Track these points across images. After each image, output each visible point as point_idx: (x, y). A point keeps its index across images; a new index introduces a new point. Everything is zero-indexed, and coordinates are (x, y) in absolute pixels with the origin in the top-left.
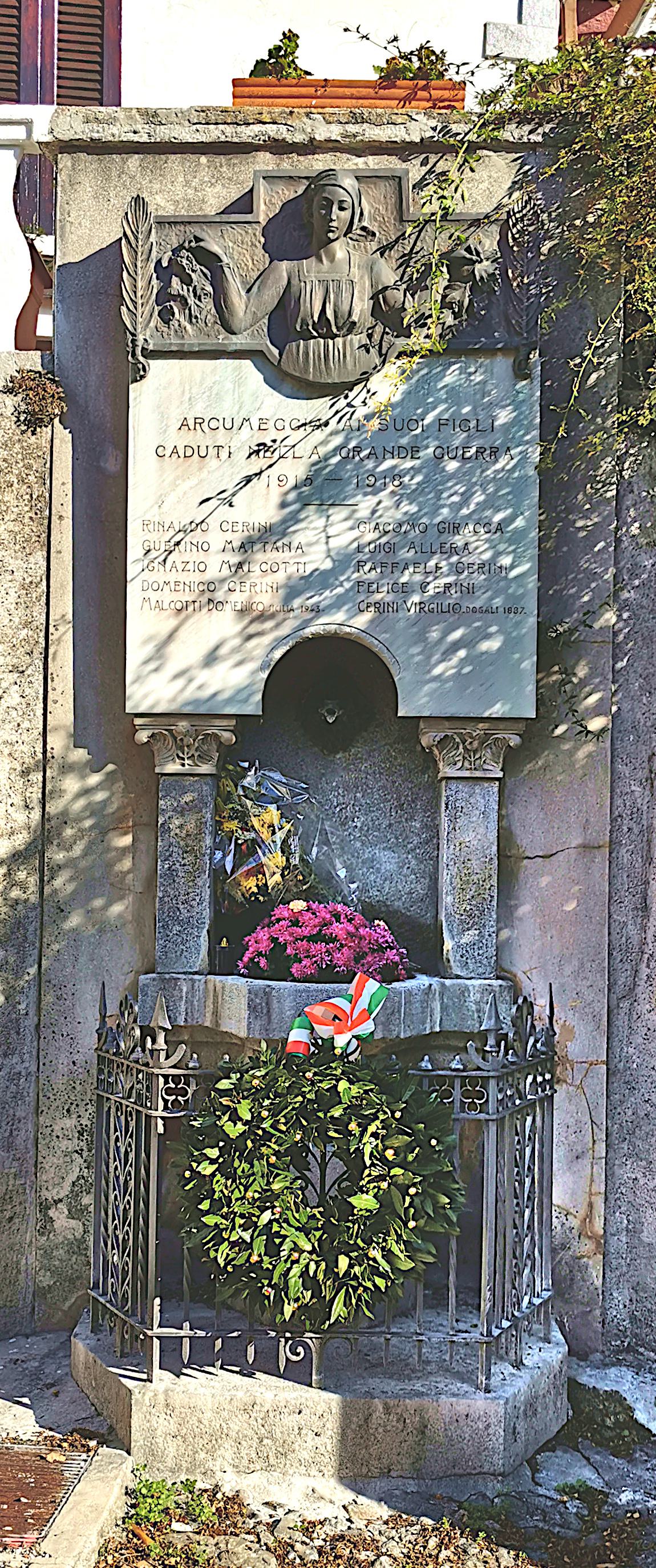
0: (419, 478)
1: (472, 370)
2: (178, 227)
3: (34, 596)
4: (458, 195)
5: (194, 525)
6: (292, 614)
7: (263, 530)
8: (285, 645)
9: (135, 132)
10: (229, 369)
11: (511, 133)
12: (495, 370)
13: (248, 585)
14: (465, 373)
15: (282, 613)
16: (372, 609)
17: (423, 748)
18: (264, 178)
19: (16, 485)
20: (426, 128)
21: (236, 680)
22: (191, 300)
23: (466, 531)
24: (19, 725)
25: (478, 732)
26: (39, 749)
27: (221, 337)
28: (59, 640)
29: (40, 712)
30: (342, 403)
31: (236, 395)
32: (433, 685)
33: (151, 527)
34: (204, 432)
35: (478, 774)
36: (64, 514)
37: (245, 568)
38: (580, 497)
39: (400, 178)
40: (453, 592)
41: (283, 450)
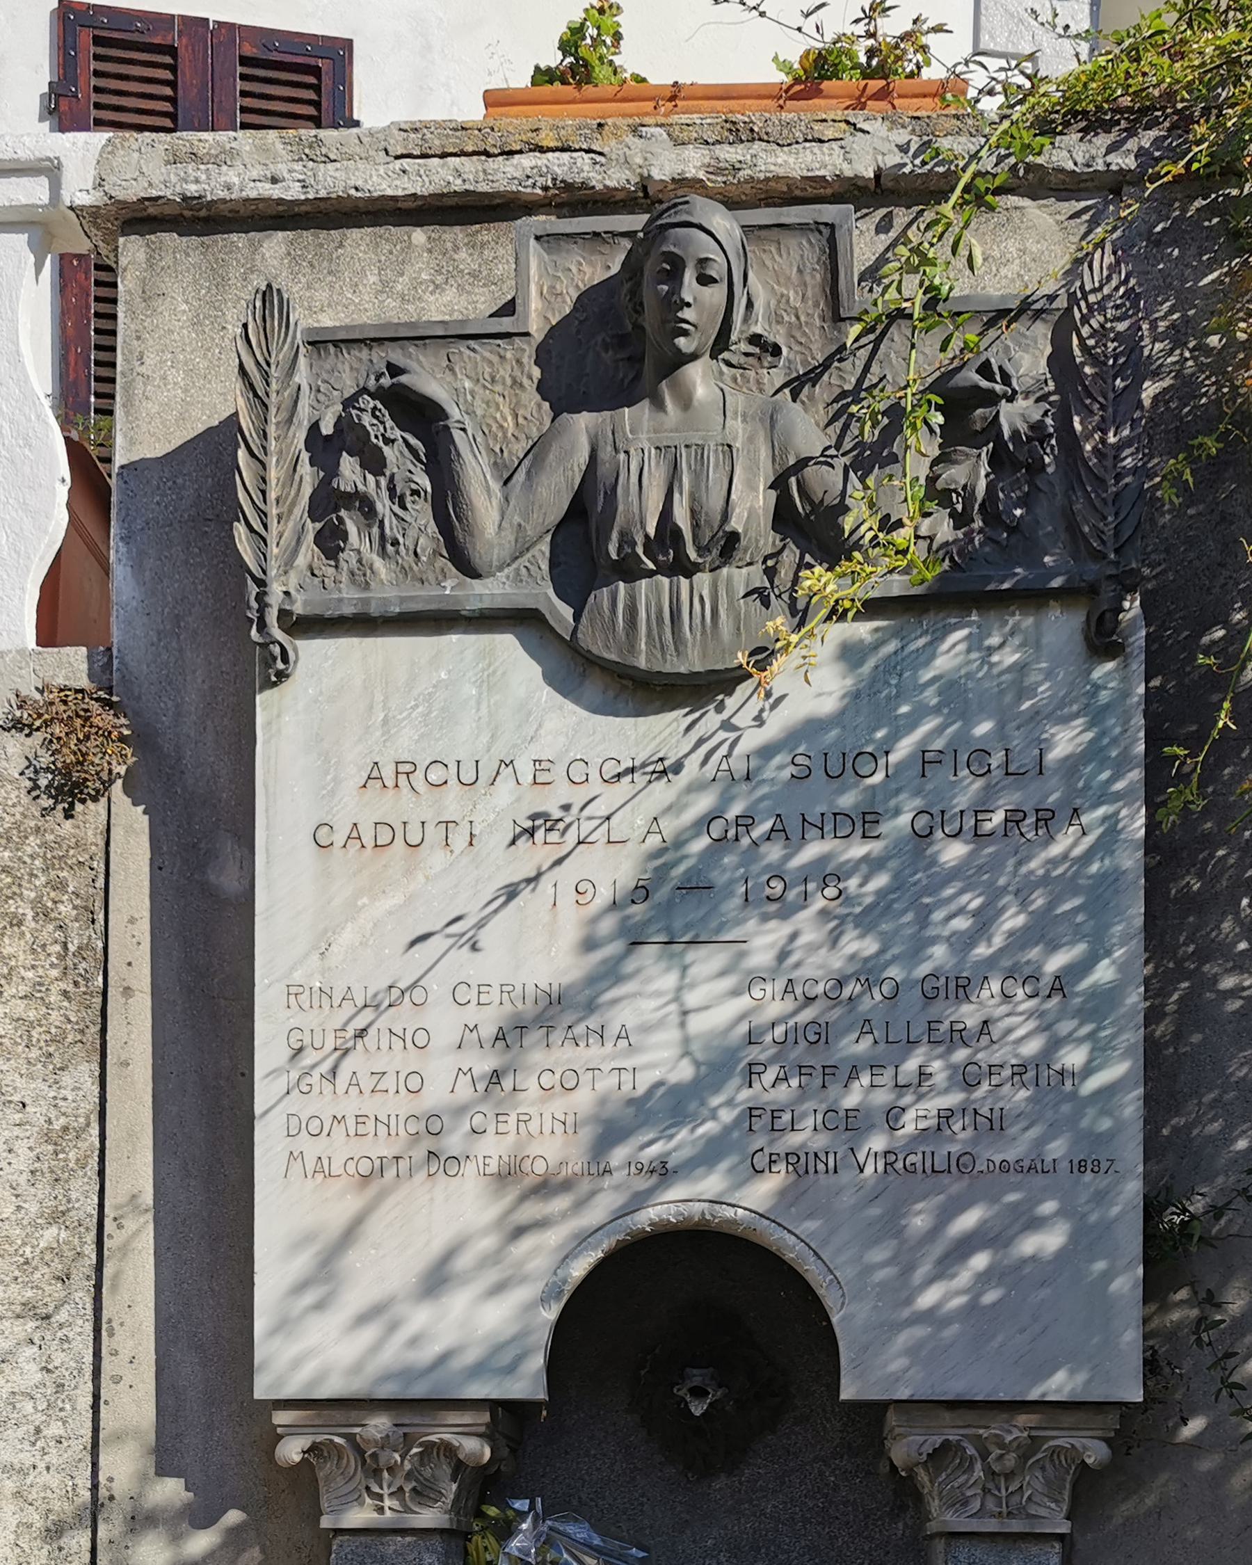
0: (881, 881)
1: (994, 640)
2: (355, 352)
3: (72, 1155)
4: (960, 262)
5: (395, 993)
6: (607, 1182)
7: (543, 1003)
8: (595, 1248)
9: (274, 180)
10: (469, 654)
11: (1070, 152)
12: (1045, 641)
13: (512, 1119)
14: (979, 649)
15: (587, 1179)
16: (782, 1167)
17: (894, 1468)
18: (538, 238)
19: (30, 923)
20: (885, 147)
21: (494, 1331)
22: (384, 506)
23: (985, 994)
24: (38, 1431)
25: (1016, 1433)
26: (84, 1481)
27: (448, 584)
28: (124, 1249)
29: (86, 1401)
30: (712, 719)
31: (484, 710)
32: (920, 1332)
33: (305, 998)
34: (434, 816)
35: (1016, 1526)
36: (134, 985)
37: (507, 1083)
38: (1226, 926)
39: (832, 227)
40: (957, 1127)
41: (587, 827)
